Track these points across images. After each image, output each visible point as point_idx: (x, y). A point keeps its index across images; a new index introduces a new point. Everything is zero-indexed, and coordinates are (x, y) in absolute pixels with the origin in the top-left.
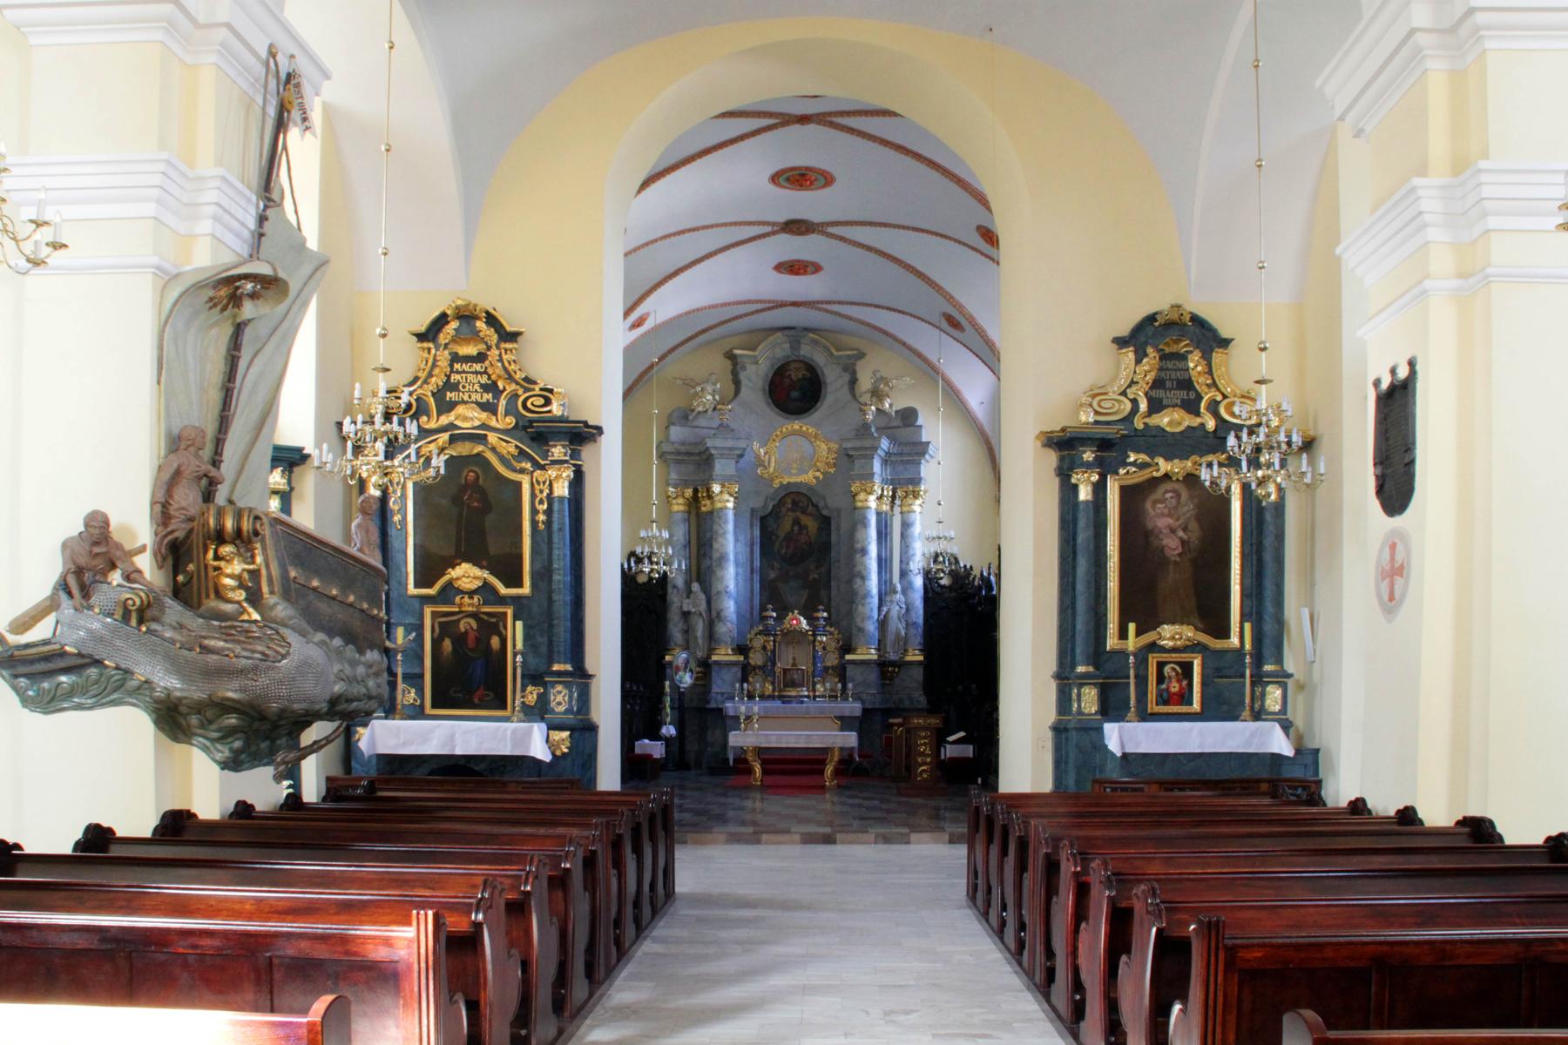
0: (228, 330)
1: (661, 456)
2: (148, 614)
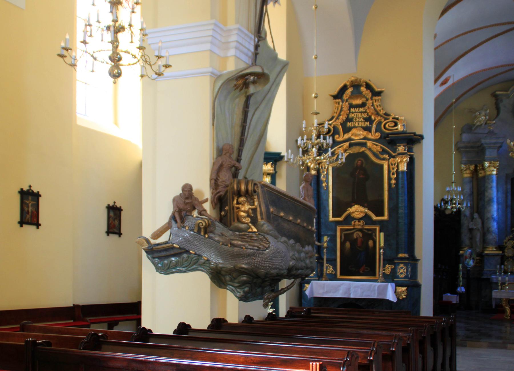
0: (243, 99)
1: (458, 149)
2: (209, 229)
